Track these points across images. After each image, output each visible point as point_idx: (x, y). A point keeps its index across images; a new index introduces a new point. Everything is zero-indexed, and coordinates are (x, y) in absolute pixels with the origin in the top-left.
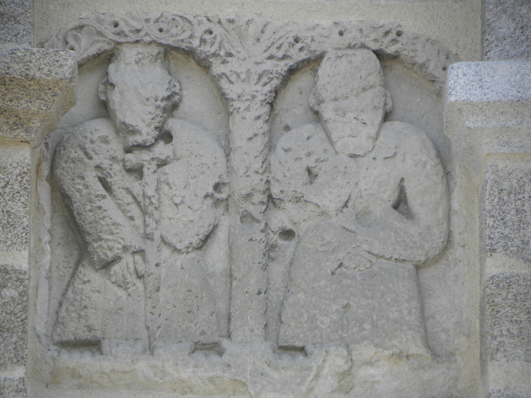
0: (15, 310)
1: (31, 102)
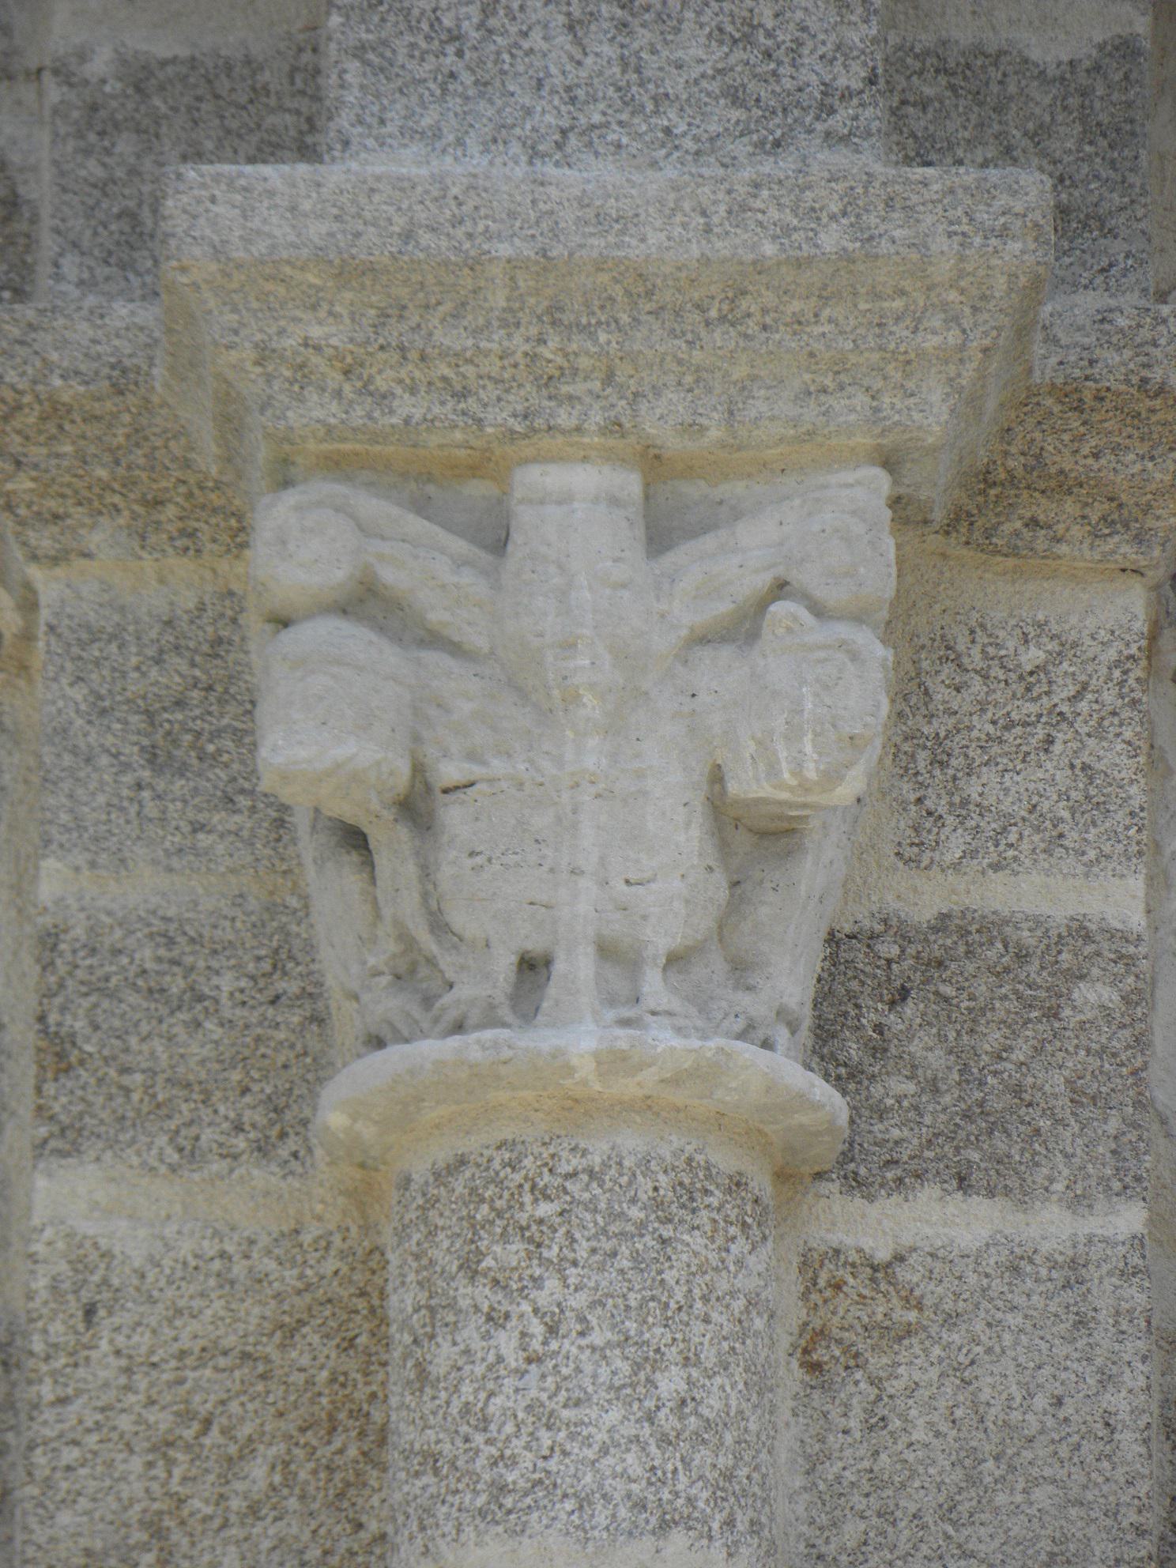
0: (1114, 1043)
1: (1152, 458)
